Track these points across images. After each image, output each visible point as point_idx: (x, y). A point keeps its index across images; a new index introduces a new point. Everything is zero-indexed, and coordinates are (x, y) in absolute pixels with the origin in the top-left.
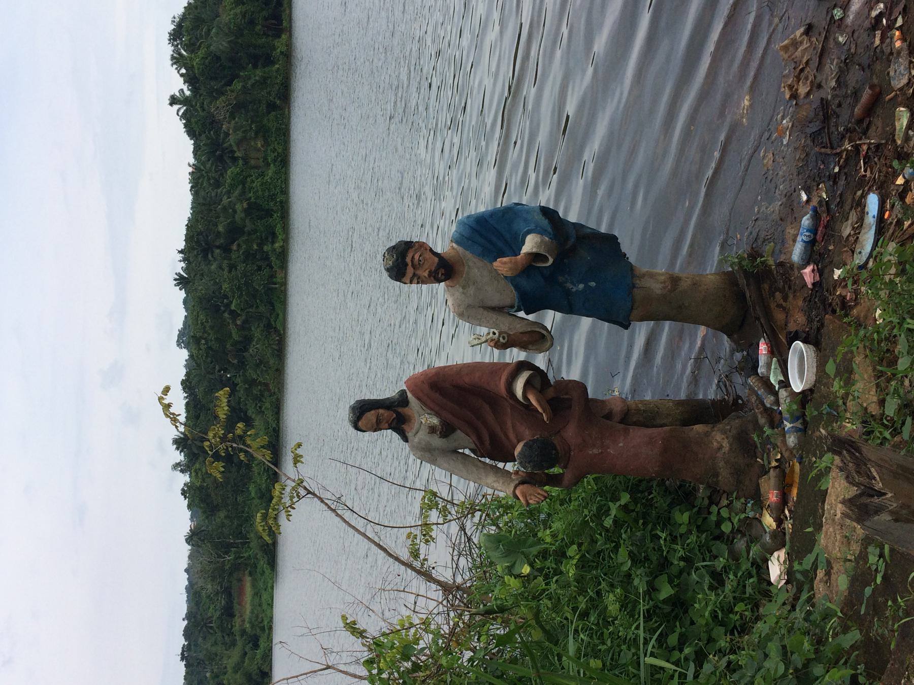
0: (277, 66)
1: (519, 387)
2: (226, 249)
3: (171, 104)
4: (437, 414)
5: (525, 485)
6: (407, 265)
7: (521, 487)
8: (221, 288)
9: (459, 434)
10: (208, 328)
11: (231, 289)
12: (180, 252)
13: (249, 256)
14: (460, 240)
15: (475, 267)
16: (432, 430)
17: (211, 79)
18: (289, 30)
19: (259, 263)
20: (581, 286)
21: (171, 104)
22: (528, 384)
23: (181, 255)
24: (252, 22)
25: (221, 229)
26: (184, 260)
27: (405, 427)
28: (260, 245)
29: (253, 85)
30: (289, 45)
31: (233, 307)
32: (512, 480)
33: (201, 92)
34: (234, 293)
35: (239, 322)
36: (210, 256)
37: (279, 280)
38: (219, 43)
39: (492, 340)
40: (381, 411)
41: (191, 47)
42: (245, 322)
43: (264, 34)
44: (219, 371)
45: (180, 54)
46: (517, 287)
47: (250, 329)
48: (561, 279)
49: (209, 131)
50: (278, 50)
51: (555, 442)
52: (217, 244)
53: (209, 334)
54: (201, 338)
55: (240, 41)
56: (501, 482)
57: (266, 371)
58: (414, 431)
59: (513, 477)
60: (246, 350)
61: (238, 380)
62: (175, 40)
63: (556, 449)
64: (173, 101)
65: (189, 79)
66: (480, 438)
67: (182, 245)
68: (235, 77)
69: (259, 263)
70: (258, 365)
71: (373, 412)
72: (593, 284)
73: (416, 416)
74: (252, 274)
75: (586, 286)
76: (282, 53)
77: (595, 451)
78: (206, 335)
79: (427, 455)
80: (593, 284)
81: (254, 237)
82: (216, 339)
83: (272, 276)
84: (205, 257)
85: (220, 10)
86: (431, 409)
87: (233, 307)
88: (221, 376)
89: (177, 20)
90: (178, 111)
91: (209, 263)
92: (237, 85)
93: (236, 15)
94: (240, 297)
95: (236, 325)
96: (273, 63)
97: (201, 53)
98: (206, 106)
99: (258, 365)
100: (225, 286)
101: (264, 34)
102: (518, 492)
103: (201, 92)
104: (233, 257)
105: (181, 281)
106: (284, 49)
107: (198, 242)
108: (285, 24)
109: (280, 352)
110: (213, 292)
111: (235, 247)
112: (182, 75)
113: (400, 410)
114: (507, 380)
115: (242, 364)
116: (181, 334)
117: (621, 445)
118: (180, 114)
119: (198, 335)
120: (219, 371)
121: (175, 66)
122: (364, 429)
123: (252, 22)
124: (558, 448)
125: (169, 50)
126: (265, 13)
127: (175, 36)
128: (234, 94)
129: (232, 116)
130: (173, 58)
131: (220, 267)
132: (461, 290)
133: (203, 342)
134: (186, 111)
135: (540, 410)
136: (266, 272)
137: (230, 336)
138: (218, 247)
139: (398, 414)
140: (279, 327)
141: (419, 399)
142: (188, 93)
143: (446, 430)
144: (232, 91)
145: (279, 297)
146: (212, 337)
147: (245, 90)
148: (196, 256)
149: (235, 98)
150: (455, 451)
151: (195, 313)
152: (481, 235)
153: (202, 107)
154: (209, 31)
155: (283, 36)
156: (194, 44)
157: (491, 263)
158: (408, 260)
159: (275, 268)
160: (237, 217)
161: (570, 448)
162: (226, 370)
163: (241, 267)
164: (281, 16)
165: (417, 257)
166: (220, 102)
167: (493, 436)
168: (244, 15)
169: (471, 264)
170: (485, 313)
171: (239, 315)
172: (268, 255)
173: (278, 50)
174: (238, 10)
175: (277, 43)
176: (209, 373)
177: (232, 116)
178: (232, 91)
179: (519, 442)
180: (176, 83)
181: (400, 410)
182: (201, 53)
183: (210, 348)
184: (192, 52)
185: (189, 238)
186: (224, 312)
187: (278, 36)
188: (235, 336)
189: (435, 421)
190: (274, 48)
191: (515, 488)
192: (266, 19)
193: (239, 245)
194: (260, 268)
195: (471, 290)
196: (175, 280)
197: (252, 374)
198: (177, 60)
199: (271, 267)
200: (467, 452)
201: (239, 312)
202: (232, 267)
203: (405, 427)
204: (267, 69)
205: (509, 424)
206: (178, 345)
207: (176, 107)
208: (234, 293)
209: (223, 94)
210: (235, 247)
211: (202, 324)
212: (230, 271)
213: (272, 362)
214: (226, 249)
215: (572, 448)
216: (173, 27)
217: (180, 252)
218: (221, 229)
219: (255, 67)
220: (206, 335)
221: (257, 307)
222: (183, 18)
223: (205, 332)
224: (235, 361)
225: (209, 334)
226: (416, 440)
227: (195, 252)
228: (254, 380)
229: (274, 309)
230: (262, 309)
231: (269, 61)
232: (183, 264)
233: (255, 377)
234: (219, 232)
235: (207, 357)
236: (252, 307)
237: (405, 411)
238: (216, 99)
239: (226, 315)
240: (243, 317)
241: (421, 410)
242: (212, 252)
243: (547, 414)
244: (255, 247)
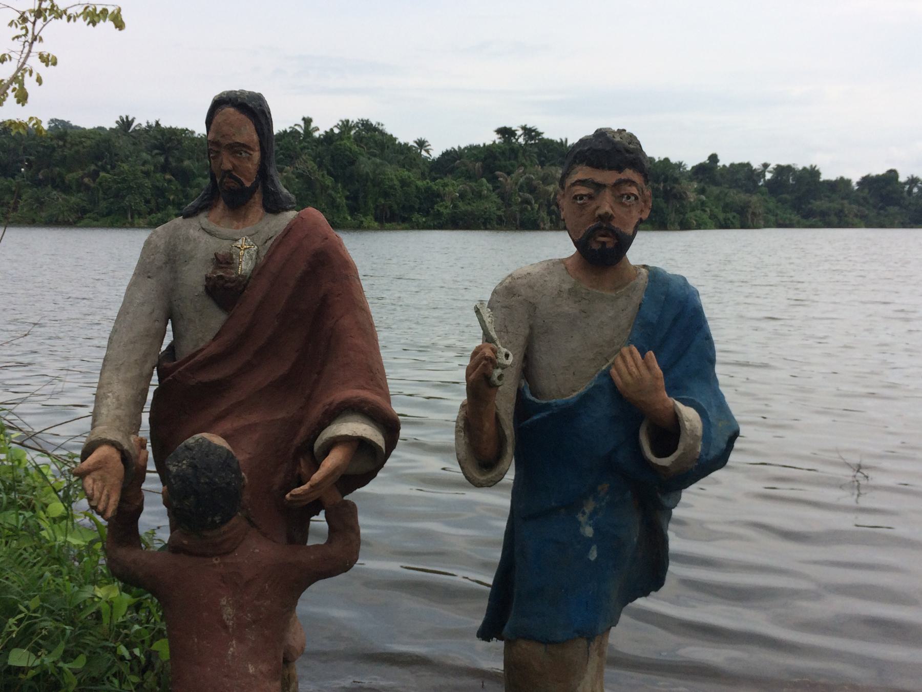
0: (349, 218)
1: (354, 427)
2: (165, 168)
3: (304, 119)
4: (259, 270)
5: (121, 466)
6: (620, 169)
7: (117, 456)
8: (123, 162)
9: (216, 319)
10: (76, 148)
11: (122, 172)
12: (157, 123)
13: (160, 192)
14: (656, 276)
15: (614, 314)
16: (224, 261)
17: (332, 156)
18: (382, 228)
19: (153, 202)
20: (589, 531)
21: (304, 119)
22: (361, 444)
23: (154, 125)
24: (386, 195)
25: (186, 163)
26: (149, 126)
27: (220, 208)
28: (173, 203)
29: (330, 195)
30: (369, 228)
31: (102, 174)
32: (128, 434)
33: (320, 147)
34: (118, 175)
35: (86, 180)
36: (156, 151)
37: (136, 221)
38: (366, 165)
39: (494, 351)
40: (256, 155)
41: (359, 139)
42: (88, 188)
43: (377, 206)
44: (28, 160)
45: (351, 128)
46: (586, 398)
47: (79, 191)
48: (604, 487)
49: (283, 154)
50: (363, 219)
51: (234, 521)
52: (171, 159)
53: (70, 149)
54: (65, 141)
55: (369, 184)
56: (119, 412)
57: (32, 209)
58: (212, 227)
59: (133, 438)
60: (55, 187)
61: (19, 179)
62: (363, 125)
63: (223, 522)
64: (307, 121)
65: (329, 136)
66: (212, 361)
67: (164, 124)
68: (336, 179)
69: (153, 202)
70: (37, 200)
71: (255, 137)
72: (593, 555)
73: (249, 229)
74: (141, 194)
75: (588, 543)
76: (362, 222)
77: (228, 613)
78: (68, 146)
79: (160, 258)
80: (593, 555)
81: (181, 196)
82: (65, 157)
83: (140, 215)
84: (155, 147)
85: (394, 166)
86: (270, 256)
87: (102, 174)
88: (22, 161)
89: (380, 128)
90: (299, 125)
91: (149, 150)
92: (329, 181)
93: (392, 180)
94: (115, 181)
95: (82, 177)
96: (351, 214)
97: (355, 148)
98: (306, 151)
99: (37, 200)
100: (125, 167)
101: (377, 206)
102: (102, 451)
103: (320, 147)
104: (158, 175)
105: (125, 124)
106: (365, 224)
107: (170, 140)
108: (387, 225)
109: (54, 222)
110: (116, 155)
111: (168, 177)
112: (332, 130)
113: (258, 197)
114: (365, 401)
115: (38, 184)
116: (65, 124)
117: (251, 669)
118: (297, 127)
119: (69, 139)
120: (28, 160)
121: (340, 123)
122: (218, 118)
123: (386, 195)
124: (225, 528)
125: (354, 118)
126: (395, 207)
127: (366, 125)
128: (320, 178)
129: (299, 176)
130: (348, 121)
131: (145, 163)
132: (566, 286)
133: (61, 143)
134: (299, 132)
135: (317, 477)
136: (143, 207)
137: (70, 171)
138: (166, 160)
139: (252, 191)
140: (86, 221)
141: (289, 231)
142: (316, 134)
143: (223, 289)
144: (323, 176)
145: (117, 221)
146: (67, 152)
147: (324, 188)
148: (155, 138)
149: (317, 179)
150: (171, 314)
151: (92, 136)
152: (675, 320)
153: (304, 148)
154: (375, 156)
155: (376, 224)
156: (361, 141)
157: (631, 341)
158: (629, 174)
159: (149, 217)
160: (201, 179)
161: (227, 553)
162: (29, 167)
163: (147, 183)
164: (394, 221)
165: (634, 190)
166: (312, 165)
167: (219, 388)
168: (392, 187)
169: (621, 302)
170: (521, 340)
171: (94, 181)
172: (163, 210)
173: (363, 219)
174: (396, 182)
175: (370, 218)
176: (24, 148)
177: (299, 176)
178: (323, 176)
179: (225, 437)
180: (324, 124)
181: (258, 197)
182: (355, 148)
183: (54, 149)
184: (355, 139)
185: (173, 132)
186: (96, 165)
187: (376, 219)
188: (70, 177)
189: (245, 266)
190: (365, 215)
191: (113, 444)
192: (390, 207)
193: (170, 181)
194: (147, 202)
195: (569, 307)
196: (127, 117)
197: (27, 194)
198: (346, 126)
199: (149, 214)
200: (168, 339)
201: (98, 180)
202: (147, 174)
203: (220, 208)
204: (345, 209)
205: (254, 418)
206: (52, 120)
207: (302, 123)
208: (118, 175)
209: (320, 167)
210: (168, 177)
211: (81, 142)
212: (143, 172)
213: (43, 214)
214: (165, 168)
215: (228, 560)
216: (374, 123)
217: (157, 123)
218: (186, 163)
219: (347, 198)
220: (68, 146)
221: (104, 199)
222: (382, 133)
223: (72, 145)
224: (41, 177)
225: (70, 149)
226: (194, 233)
227: (159, 137)
228: (19, 197)
229: (104, 216)
230: (103, 205)
231: (353, 210)
232: (144, 125)
233: (24, 197)
234: (182, 161)
235: (43, 146)
236: (105, 193)
237: (256, 208)
238: (314, 161)
239: (93, 167)
240: (92, 185)
241: (263, 237)
242: (161, 154)
243: (306, 493)
244: (172, 197)
